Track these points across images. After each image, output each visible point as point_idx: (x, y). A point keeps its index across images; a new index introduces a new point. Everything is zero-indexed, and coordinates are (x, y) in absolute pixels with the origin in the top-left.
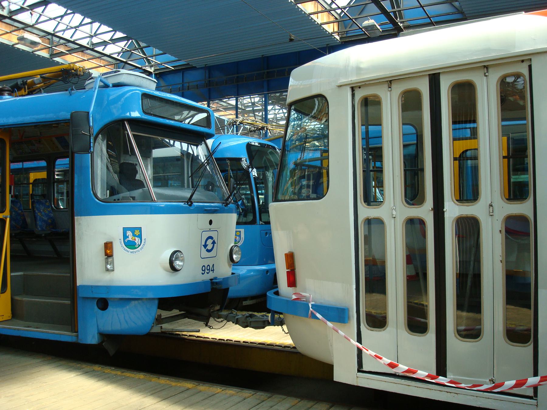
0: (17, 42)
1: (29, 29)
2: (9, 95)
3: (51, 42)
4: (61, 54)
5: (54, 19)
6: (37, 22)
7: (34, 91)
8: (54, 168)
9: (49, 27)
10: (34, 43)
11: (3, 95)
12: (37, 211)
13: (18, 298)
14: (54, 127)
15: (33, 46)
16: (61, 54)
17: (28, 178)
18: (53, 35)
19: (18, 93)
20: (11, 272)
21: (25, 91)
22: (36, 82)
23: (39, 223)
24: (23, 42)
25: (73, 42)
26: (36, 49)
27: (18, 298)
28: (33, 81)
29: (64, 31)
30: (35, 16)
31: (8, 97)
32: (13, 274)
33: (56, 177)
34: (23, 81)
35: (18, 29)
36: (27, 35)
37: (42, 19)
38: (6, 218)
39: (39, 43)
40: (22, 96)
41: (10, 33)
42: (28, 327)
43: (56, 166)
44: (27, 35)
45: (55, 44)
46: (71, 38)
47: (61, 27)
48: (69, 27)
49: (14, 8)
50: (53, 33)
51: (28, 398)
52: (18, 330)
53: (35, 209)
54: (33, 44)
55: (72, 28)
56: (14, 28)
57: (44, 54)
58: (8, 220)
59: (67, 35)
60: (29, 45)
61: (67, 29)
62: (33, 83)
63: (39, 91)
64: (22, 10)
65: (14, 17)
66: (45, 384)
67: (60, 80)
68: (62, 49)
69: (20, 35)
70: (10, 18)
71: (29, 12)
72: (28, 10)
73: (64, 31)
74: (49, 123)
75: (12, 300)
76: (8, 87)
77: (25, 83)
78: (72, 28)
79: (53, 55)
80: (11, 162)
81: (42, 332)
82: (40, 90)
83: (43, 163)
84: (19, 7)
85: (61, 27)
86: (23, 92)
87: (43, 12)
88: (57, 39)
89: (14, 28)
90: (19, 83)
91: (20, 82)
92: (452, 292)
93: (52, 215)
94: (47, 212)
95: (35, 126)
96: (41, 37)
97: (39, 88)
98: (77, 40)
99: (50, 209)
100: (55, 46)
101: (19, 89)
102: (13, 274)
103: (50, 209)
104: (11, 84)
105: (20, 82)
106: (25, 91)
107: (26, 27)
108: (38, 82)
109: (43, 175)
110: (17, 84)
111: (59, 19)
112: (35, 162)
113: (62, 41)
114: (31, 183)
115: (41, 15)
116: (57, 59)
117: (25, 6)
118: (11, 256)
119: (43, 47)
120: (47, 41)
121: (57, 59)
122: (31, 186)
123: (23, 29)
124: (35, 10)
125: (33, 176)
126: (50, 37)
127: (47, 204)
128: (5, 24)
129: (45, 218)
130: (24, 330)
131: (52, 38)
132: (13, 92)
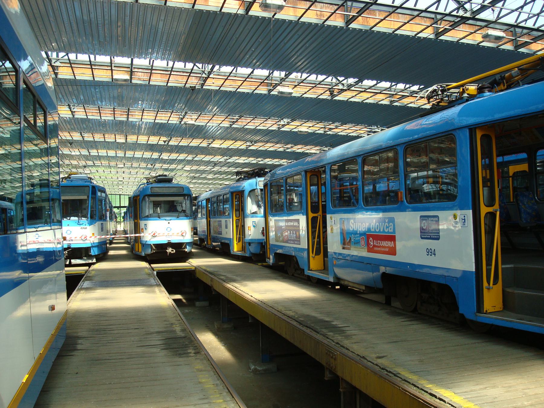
0: (481, 40)
1: (491, 26)
2: (489, 91)
3: (514, 34)
4: (526, 44)
5: (516, 10)
6: (498, 18)
7: (512, 84)
8: (536, 159)
9: (510, 19)
10: (498, 38)
11: (483, 92)
12: (521, 204)
13: (508, 290)
14: (540, 117)
15: (497, 41)
16: (526, 44)
17: (508, 172)
18: (517, 26)
19: (498, 88)
20: (502, 264)
21: (504, 86)
22: (514, 75)
23: (523, 215)
24: (488, 39)
25: (538, 30)
26: (500, 43)
27: (508, 290)
28: (511, 75)
29: (526, 20)
30: (497, 10)
31: (488, 94)
32: (503, 266)
33: (538, 168)
34: (501, 76)
35: (482, 28)
36: (491, 32)
37: (504, 12)
38: (496, 211)
39: (503, 37)
40: (502, 91)
41: (475, 32)
42: (521, 319)
43: (538, 158)
44: (491, 32)
45: (518, 35)
46: (445, 11)
47: (523, 17)
48: (531, 15)
49: (476, 7)
50: (516, 24)
51: (525, 391)
52: (511, 321)
53: (519, 202)
54: (498, 38)
55: (534, 15)
56: (477, 28)
57: (509, 47)
58: (498, 213)
59: (530, 24)
60: (494, 41)
61: (529, 18)
62: (511, 77)
63: (517, 84)
64: (483, 8)
65: (476, 17)
66: (540, 379)
67: (538, 70)
68: (525, 39)
69: (484, 33)
70: (473, 19)
71: (490, 9)
72: (490, 7)
73: (526, 20)
74: (534, 114)
75: (504, 292)
76: (486, 84)
77: (503, 78)
78: (534, 15)
79: (517, 47)
80: (498, 156)
81: (535, 326)
82: (519, 83)
83: (524, 156)
84: (479, 7)
85: (523, 17)
86: (502, 87)
87: (503, 5)
88: (520, 30)
89: (477, 28)
90: (497, 79)
91: (498, 77)
92: (10, 277)
93: (536, 207)
94: (531, 205)
95: (521, 118)
96: (505, 31)
97: (517, 81)
98: (541, 27)
99: (533, 201)
100: (519, 37)
101: (498, 84)
102: (503, 266)
103: (533, 201)
104: (490, 81)
105: (498, 77)
106: (504, 86)
107: (488, 23)
108: (516, 74)
109: (524, 167)
110: (495, 79)
111: (520, 10)
112: (514, 155)
113: (525, 31)
114: (511, 177)
115: (501, 9)
116: (522, 50)
117: (486, 3)
118: (502, 249)
119: (506, 40)
120: (510, 33)
121: (522, 50)
122: (511, 179)
123: (486, 26)
124: (497, 5)
125: (512, 169)
126: (512, 29)
127: (531, 196)
128: (468, 26)
129: (529, 211)
130: (517, 322)
131: (515, 30)
132: (492, 88)
